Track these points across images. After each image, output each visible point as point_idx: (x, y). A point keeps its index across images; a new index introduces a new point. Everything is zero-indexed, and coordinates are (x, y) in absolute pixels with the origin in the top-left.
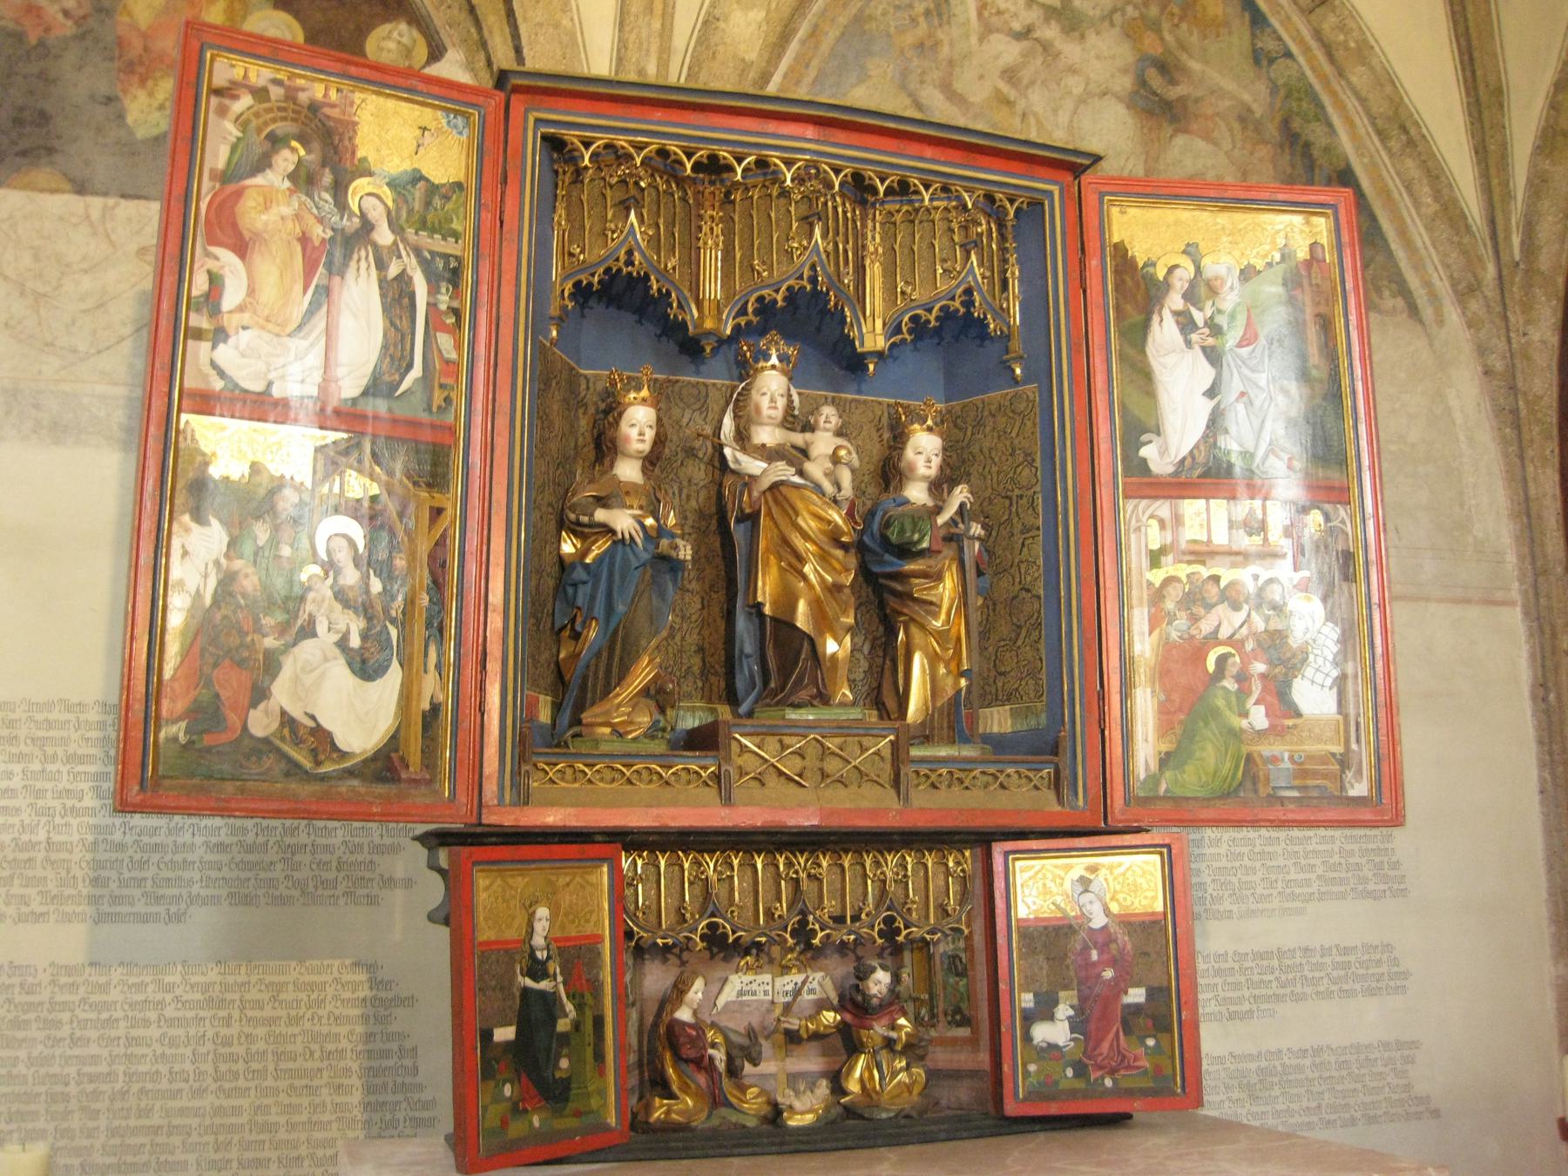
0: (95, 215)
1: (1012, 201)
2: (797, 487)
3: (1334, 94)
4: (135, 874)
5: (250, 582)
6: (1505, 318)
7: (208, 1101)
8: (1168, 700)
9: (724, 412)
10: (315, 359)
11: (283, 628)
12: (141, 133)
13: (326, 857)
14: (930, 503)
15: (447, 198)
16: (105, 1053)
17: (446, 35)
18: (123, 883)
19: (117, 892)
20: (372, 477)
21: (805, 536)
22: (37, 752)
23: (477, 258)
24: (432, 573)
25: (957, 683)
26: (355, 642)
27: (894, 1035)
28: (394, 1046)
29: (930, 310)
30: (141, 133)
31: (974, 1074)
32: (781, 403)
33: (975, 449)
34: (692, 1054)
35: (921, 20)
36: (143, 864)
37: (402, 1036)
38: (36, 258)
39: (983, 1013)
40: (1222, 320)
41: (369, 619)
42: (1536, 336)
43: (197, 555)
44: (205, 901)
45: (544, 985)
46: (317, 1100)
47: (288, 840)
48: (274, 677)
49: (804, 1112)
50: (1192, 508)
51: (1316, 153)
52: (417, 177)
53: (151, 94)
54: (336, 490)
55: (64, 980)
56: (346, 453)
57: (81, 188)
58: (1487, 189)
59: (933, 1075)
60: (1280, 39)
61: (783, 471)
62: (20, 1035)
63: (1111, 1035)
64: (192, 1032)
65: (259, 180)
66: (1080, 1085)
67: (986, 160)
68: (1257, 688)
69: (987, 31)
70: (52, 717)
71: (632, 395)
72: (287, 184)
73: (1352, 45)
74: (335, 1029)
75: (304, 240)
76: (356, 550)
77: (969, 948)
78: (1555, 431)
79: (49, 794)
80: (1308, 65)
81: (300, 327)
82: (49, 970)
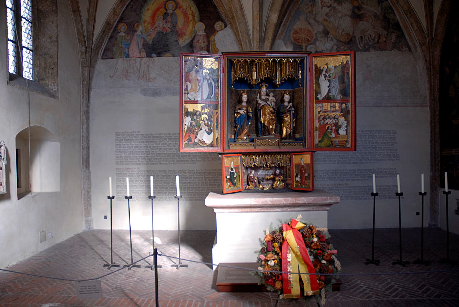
0: (176, 60)
5: (194, 123)
7: (200, 189)
12: (182, 46)
17: (228, 23)
18: (187, 159)
26: (207, 130)
30: (182, 46)
34: (252, 180)
36: (190, 156)
40: (331, 75)
42: (436, 53)
44: (199, 161)
45: (233, 171)
50: (325, 104)
51: (390, 20)
68: (333, 131)
69: (323, 6)
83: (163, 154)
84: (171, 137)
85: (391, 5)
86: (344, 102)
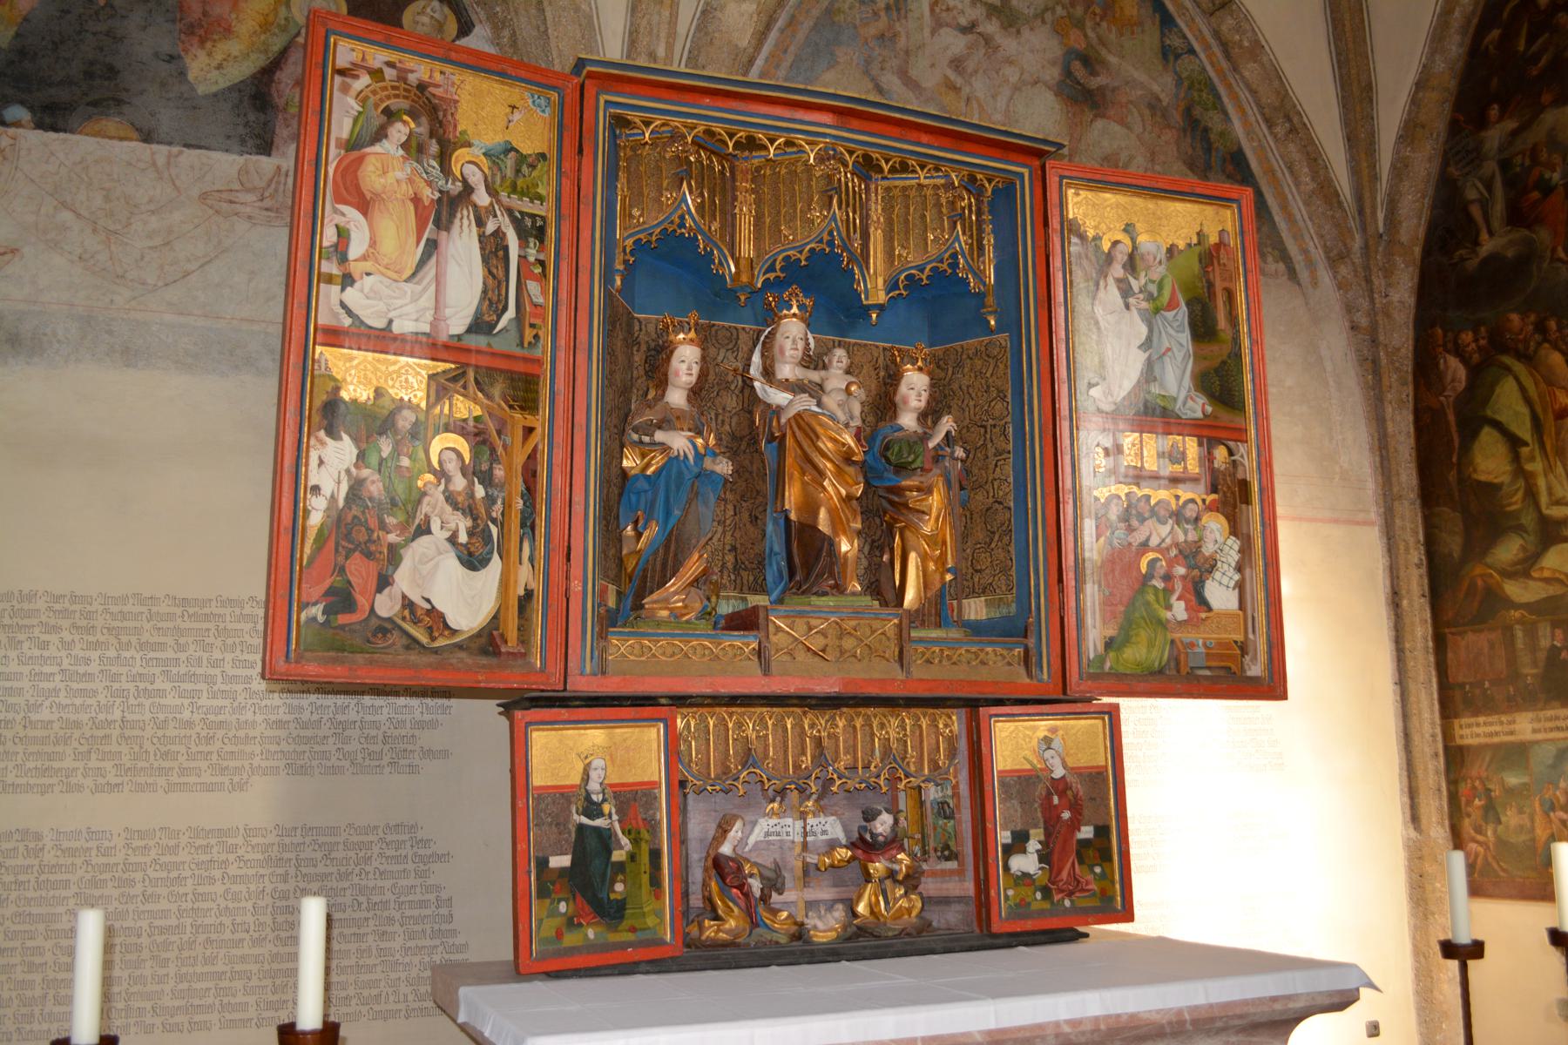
0: (161, 161)
1: (990, 181)
2: (815, 414)
3: (1229, 87)
4: (201, 748)
5: (375, 488)
6: (1368, 281)
8: (1111, 594)
9: (751, 352)
10: (427, 300)
11: (403, 527)
12: (201, 90)
13: (373, 733)
14: (920, 431)
15: (533, 166)
16: (174, 907)
19: (185, 765)
20: (475, 401)
21: (824, 455)
22: (113, 640)
23: (559, 217)
24: (525, 482)
25: (943, 578)
26: (463, 538)
27: (896, 867)
28: (432, 897)
29: (922, 271)
30: (201, 90)
31: (960, 899)
32: (801, 345)
33: (955, 386)
35: (882, 14)
36: (209, 739)
37: (438, 888)
38: (107, 199)
39: (968, 849)
41: (475, 519)
43: (332, 463)
45: (599, 822)
46: (364, 946)
47: (340, 717)
48: (397, 566)
49: (825, 927)
52: (509, 149)
53: (210, 54)
54: (446, 410)
55: (137, 843)
56: (454, 379)
57: (147, 137)
58: (1355, 171)
59: (926, 901)
60: (1185, 37)
61: (805, 403)
62: (97, 893)
63: (1069, 865)
64: (253, 887)
65: (377, 148)
66: (1047, 906)
67: (967, 146)
69: (938, 25)
70: (125, 609)
71: (681, 336)
72: (401, 152)
73: (1246, 44)
74: (380, 883)
75: (416, 200)
76: (463, 460)
77: (956, 795)
78: (1410, 378)
79: (124, 678)
80: (1208, 60)
81: (414, 275)
82: (124, 835)
83: (28, 724)
84: (89, 615)
85: (1212, 74)
86: (1223, 435)
